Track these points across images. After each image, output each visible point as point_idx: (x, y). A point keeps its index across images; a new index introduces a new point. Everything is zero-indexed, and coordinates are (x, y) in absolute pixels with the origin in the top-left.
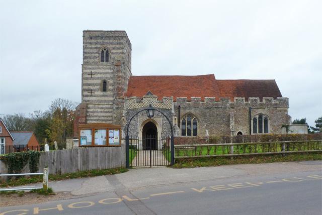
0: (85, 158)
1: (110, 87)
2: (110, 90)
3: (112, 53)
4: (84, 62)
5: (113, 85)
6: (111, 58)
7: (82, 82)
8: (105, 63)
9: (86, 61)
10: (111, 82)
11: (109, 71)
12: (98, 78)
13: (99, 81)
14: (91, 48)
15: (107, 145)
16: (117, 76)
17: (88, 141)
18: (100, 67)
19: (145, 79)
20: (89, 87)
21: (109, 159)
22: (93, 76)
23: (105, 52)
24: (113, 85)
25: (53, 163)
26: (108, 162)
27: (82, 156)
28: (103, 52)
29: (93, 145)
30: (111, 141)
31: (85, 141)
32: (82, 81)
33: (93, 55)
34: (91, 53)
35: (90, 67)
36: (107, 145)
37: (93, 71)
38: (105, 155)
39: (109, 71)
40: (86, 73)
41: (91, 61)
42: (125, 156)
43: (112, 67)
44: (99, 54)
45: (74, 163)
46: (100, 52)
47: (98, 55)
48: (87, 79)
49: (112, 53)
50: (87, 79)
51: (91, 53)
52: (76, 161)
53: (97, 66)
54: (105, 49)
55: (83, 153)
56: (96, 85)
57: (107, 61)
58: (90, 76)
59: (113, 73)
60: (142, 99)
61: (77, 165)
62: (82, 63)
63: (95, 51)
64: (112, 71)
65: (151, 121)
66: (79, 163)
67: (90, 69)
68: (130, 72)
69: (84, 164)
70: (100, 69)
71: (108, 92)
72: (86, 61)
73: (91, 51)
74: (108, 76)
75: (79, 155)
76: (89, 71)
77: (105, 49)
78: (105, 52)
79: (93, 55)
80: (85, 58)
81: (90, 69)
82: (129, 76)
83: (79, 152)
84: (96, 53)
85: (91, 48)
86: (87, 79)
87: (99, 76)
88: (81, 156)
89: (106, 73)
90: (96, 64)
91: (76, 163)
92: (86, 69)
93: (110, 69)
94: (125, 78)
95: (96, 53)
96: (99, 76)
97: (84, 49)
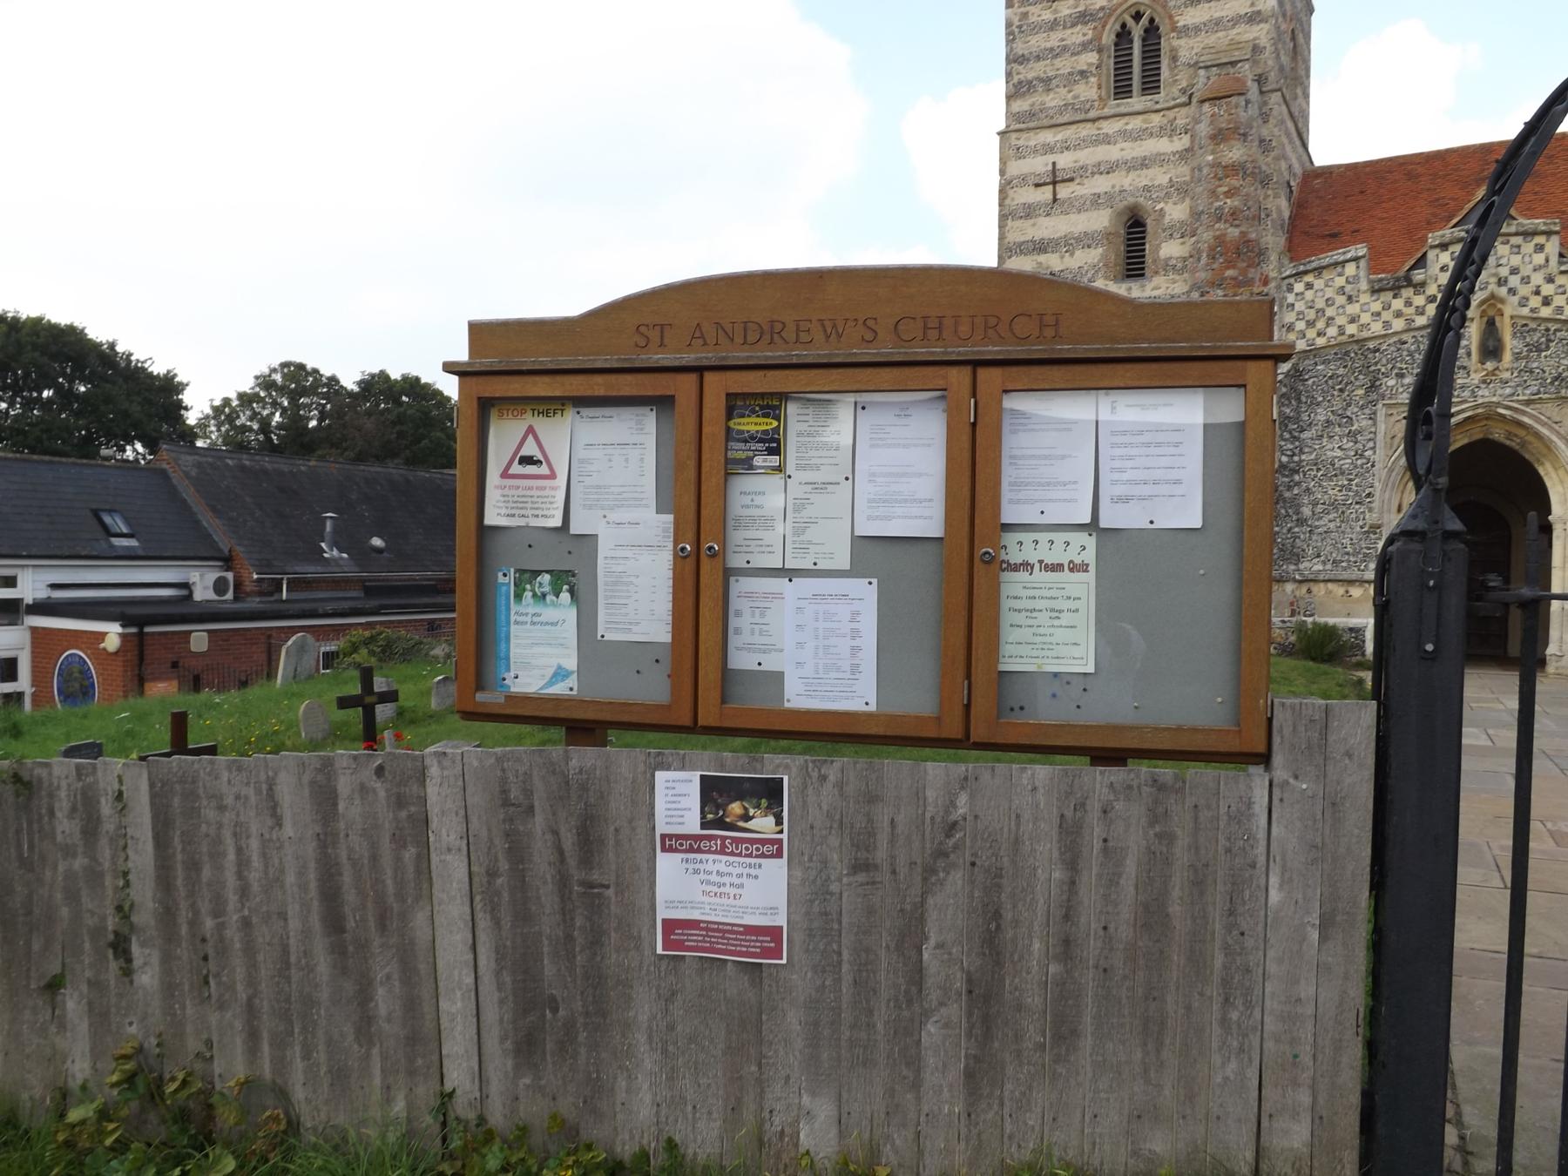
0: (548, 923)
1: (1171, 249)
2: (1167, 267)
3: (1185, 31)
4: (1010, 115)
5: (1185, 231)
6: (1174, 59)
7: (1001, 238)
8: (1137, 102)
9: (1021, 105)
10: (1176, 212)
11: (1164, 145)
12: (1096, 201)
13: (1100, 220)
14: (1053, 25)
15: (967, 706)
16: (1216, 165)
17: (610, 628)
18: (1109, 127)
19: (1410, 176)
20: (1042, 258)
21: (985, 999)
22: (1064, 192)
23: (1137, 32)
24: (1185, 231)
25: (120, 947)
26: (978, 1078)
27: (503, 888)
28: (1123, 35)
29: (701, 701)
30: (1053, 632)
31: (562, 612)
32: (1001, 227)
33: (1065, 65)
34: (1055, 53)
35: (1048, 137)
36: (967, 706)
37: (1065, 161)
38: (911, 933)
39: (1164, 145)
40: (1023, 180)
41: (1052, 100)
42: (1357, 994)
43: (1182, 117)
44: (1100, 51)
45: (385, 1001)
46: (1108, 38)
47: (1092, 57)
48: (1029, 212)
49: (1185, 31)
50: (1029, 212)
51: (1055, 53)
52: (416, 969)
53: (1086, 130)
54: (1137, 16)
55: (517, 852)
56: (1084, 240)
57: (1151, 84)
58: (1045, 194)
59: (1185, 155)
60: (1421, 262)
61: (422, 1039)
62: (1002, 126)
63: (1077, 35)
64: (1182, 142)
65: (1498, 434)
66: (454, 1007)
67: (1049, 149)
68: (1305, 146)
69: (527, 1048)
70: (1107, 140)
71: (1157, 280)
72: (1021, 105)
73: (1054, 40)
74: (1160, 176)
75: (451, 871)
76: (1039, 165)
77: (1137, 16)
78: (1137, 32)
79: (1065, 65)
80: (1016, 91)
81: (1049, 149)
82: (1298, 169)
83: (445, 831)
84: (1085, 47)
85: (1053, 25)
86: (1028, 216)
87: (1101, 184)
88: (480, 890)
89: (1144, 163)
90: (1082, 116)
91: (411, 1006)
92: (1020, 153)
93: (1170, 131)
94: (1265, 181)
95: (1085, 47)
96: (1101, 184)
97: (1011, 37)
